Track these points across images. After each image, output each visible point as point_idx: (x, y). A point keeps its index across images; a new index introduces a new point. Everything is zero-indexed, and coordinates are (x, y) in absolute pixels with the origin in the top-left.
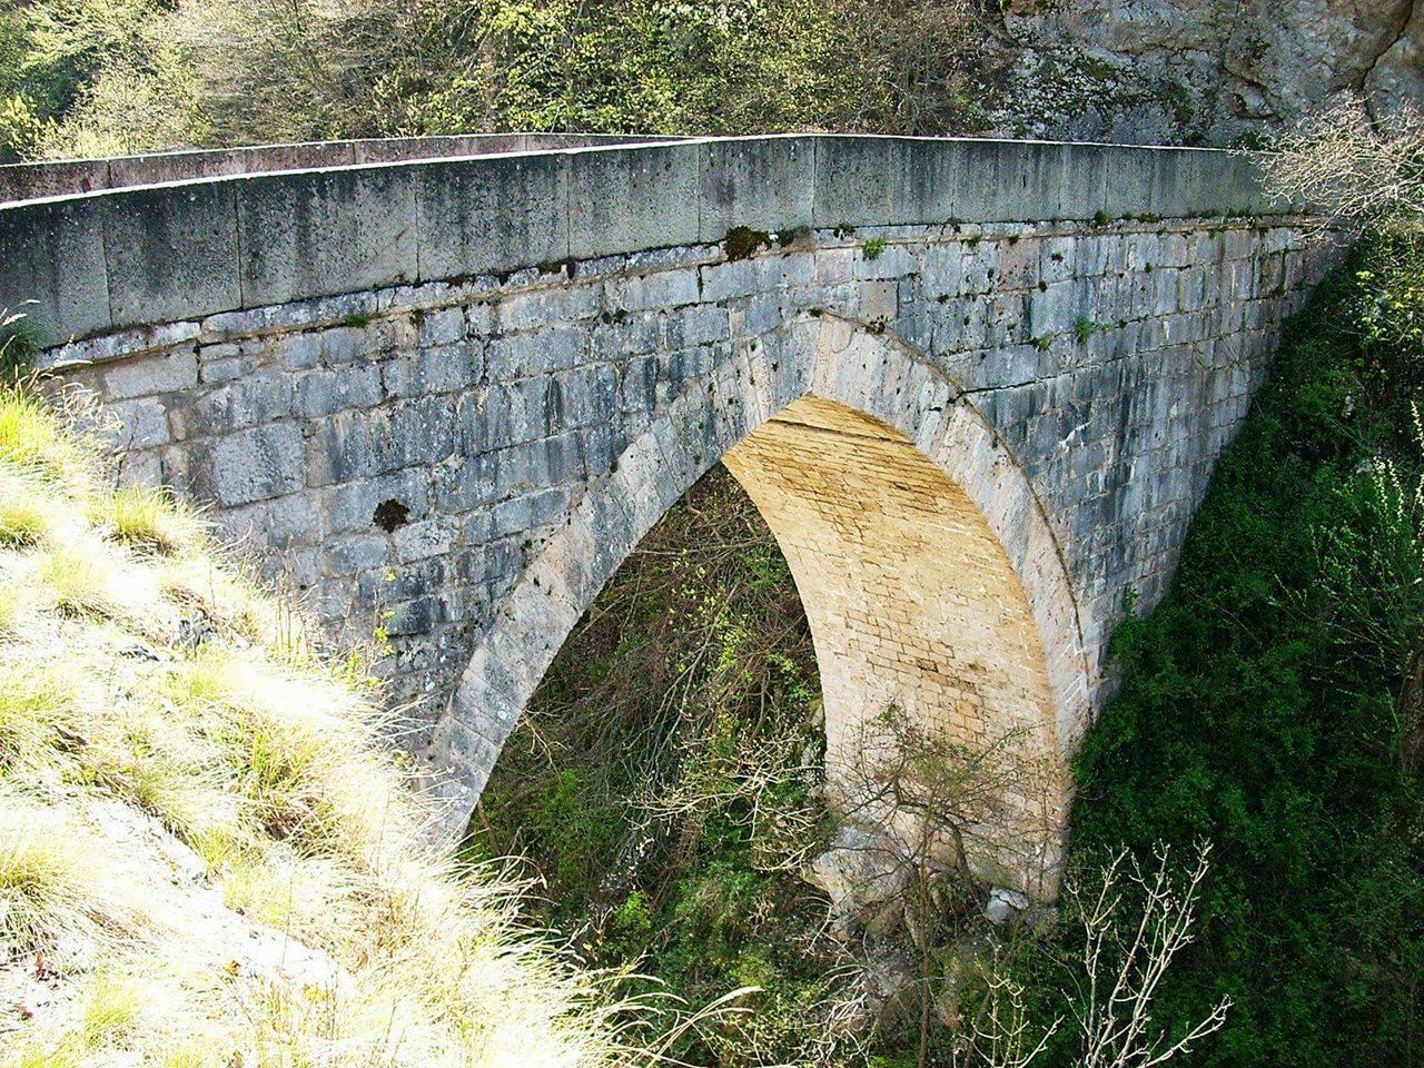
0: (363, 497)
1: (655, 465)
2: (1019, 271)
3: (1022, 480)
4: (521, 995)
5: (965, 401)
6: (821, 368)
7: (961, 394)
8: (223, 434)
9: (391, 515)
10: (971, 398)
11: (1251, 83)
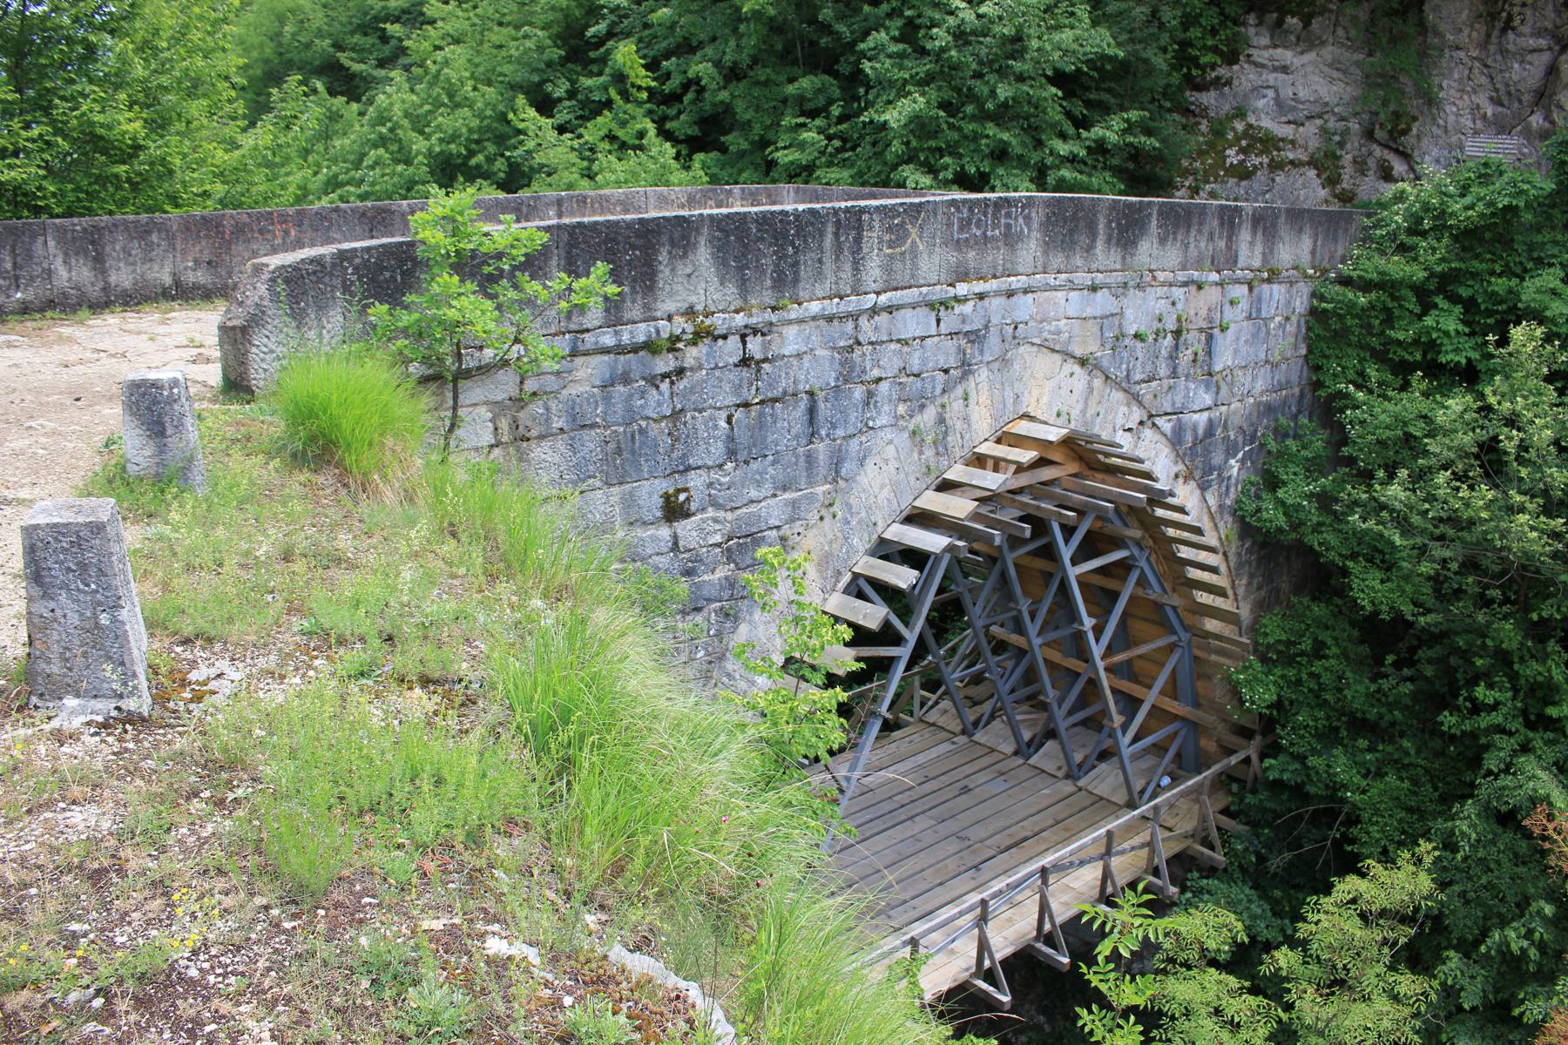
0: (650, 493)
1: (893, 471)
2: (1203, 313)
3: (1198, 492)
4: (179, 582)
5: (1154, 424)
6: (1035, 392)
7: (1151, 416)
8: (541, 437)
9: (674, 511)
10: (1159, 421)
11: (1397, 151)
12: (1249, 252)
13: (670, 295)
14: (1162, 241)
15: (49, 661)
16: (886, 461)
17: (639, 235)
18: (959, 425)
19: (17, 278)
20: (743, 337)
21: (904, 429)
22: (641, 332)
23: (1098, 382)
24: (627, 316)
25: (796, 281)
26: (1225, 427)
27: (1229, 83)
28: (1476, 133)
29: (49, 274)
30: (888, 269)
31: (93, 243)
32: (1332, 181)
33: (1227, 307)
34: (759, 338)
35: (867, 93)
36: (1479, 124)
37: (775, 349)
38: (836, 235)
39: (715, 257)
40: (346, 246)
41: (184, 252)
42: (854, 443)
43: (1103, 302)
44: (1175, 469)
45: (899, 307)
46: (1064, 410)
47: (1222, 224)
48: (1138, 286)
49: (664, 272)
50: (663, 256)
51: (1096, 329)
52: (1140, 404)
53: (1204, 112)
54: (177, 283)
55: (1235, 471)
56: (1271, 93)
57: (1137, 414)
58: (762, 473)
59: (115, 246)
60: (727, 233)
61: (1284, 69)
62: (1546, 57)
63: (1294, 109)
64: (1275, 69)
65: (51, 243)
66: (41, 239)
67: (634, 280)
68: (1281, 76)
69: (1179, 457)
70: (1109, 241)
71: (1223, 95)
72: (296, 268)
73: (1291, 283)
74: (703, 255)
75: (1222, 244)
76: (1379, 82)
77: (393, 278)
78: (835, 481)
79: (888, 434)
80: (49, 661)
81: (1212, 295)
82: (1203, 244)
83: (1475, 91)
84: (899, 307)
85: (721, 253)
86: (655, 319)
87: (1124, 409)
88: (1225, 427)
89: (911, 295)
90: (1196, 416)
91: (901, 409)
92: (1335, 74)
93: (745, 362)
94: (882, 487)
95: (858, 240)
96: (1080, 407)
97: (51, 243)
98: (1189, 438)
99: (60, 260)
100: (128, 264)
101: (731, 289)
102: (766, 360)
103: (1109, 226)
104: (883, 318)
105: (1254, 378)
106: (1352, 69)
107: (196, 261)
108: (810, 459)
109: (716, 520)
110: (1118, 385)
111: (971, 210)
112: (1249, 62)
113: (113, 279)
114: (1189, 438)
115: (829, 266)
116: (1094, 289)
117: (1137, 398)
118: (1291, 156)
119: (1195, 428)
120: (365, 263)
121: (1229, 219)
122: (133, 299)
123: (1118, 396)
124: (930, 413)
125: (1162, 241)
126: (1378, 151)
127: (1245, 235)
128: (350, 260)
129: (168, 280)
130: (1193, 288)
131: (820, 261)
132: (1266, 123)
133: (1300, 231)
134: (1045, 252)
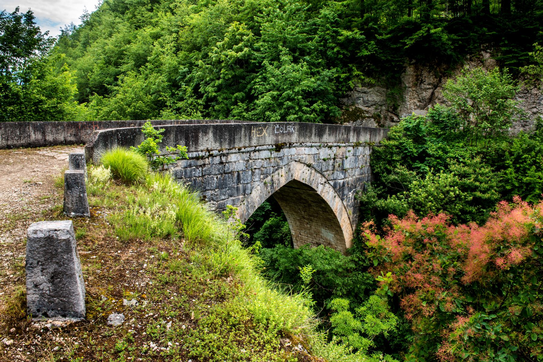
2: (341, 154)
3: (341, 201)
6: (297, 173)
10: (330, 182)
12: (353, 138)
13: (202, 145)
14: (329, 135)
15: (68, 204)
16: (258, 190)
17: (194, 129)
18: (277, 181)
19: (20, 137)
20: (221, 157)
21: (262, 182)
22: (195, 154)
23: (313, 171)
24: (191, 150)
25: (234, 143)
26: (348, 184)
27: (350, 96)
28: (415, 109)
29: (29, 136)
30: (258, 140)
31: (42, 128)
32: (379, 122)
33: (347, 152)
34: (225, 157)
35: (454, 131)
36: (416, 107)
37: (229, 160)
38: (245, 131)
39: (214, 136)
40: (118, 129)
41: (67, 132)
42: (249, 185)
43: (314, 151)
44: (334, 195)
45: (261, 150)
46: (305, 178)
47: (345, 131)
48: (323, 147)
49: (200, 139)
50: (200, 135)
51: (313, 157)
52: (325, 177)
53: (344, 104)
54: (65, 140)
55: (351, 196)
56: (362, 99)
57: (324, 180)
58: (226, 192)
59: (49, 129)
60: (217, 130)
61: (365, 93)
62: (431, 91)
63: (367, 103)
64: (363, 93)
65: (31, 128)
66: (28, 127)
67: (193, 141)
68: (364, 94)
69: (336, 192)
70: (315, 134)
71: (349, 99)
72: (105, 133)
73: (364, 147)
74: (211, 135)
75: (346, 136)
76: (391, 97)
77: (131, 137)
78: (244, 195)
79: (258, 183)
80: (68, 204)
81: (343, 149)
82: (340, 136)
83: (414, 99)
84: (261, 150)
85: (215, 134)
86: (198, 151)
87: (320, 178)
88: (348, 184)
89: (265, 147)
90: (340, 181)
91: (262, 177)
92: (378, 94)
93: (221, 163)
94: (257, 197)
95: (250, 132)
96: (309, 178)
97: (31, 128)
98: (338, 187)
99: (33, 132)
100: (52, 134)
101: (218, 144)
102: (227, 163)
103: (315, 130)
104: (257, 153)
105: (355, 171)
106: (383, 93)
107: (71, 134)
108: (238, 189)
109: (213, 204)
110: (319, 172)
111: (279, 126)
112: (356, 91)
113: (47, 138)
114: (338, 187)
115: (243, 139)
116: (312, 146)
117: (323, 176)
118: (367, 115)
119: (340, 183)
120: (123, 133)
121: (348, 129)
122: (54, 144)
123: (319, 175)
124: (269, 178)
125: (329, 135)
126: (390, 114)
127: (352, 134)
128: (119, 132)
129: (62, 139)
130: (338, 148)
131: (241, 138)
132: (360, 107)
133: (366, 133)
134: (299, 137)
